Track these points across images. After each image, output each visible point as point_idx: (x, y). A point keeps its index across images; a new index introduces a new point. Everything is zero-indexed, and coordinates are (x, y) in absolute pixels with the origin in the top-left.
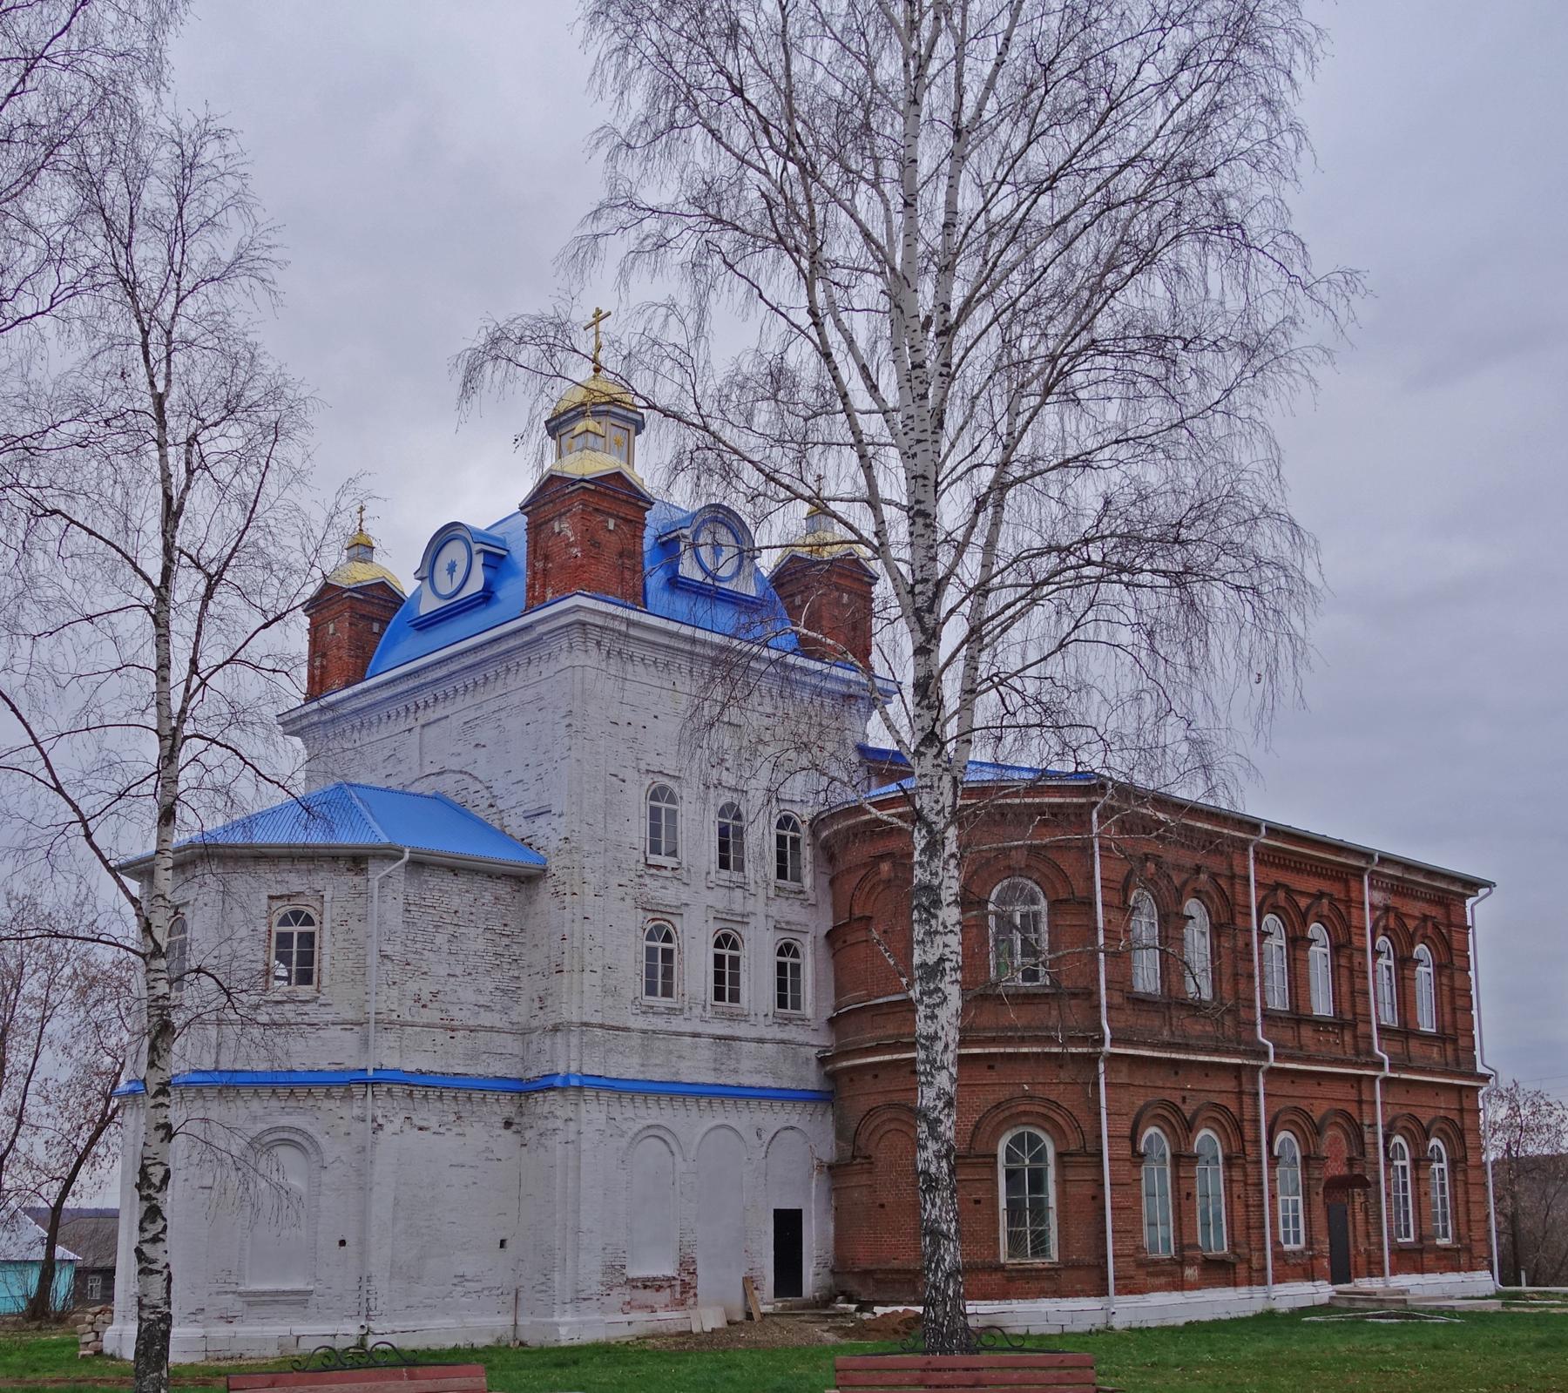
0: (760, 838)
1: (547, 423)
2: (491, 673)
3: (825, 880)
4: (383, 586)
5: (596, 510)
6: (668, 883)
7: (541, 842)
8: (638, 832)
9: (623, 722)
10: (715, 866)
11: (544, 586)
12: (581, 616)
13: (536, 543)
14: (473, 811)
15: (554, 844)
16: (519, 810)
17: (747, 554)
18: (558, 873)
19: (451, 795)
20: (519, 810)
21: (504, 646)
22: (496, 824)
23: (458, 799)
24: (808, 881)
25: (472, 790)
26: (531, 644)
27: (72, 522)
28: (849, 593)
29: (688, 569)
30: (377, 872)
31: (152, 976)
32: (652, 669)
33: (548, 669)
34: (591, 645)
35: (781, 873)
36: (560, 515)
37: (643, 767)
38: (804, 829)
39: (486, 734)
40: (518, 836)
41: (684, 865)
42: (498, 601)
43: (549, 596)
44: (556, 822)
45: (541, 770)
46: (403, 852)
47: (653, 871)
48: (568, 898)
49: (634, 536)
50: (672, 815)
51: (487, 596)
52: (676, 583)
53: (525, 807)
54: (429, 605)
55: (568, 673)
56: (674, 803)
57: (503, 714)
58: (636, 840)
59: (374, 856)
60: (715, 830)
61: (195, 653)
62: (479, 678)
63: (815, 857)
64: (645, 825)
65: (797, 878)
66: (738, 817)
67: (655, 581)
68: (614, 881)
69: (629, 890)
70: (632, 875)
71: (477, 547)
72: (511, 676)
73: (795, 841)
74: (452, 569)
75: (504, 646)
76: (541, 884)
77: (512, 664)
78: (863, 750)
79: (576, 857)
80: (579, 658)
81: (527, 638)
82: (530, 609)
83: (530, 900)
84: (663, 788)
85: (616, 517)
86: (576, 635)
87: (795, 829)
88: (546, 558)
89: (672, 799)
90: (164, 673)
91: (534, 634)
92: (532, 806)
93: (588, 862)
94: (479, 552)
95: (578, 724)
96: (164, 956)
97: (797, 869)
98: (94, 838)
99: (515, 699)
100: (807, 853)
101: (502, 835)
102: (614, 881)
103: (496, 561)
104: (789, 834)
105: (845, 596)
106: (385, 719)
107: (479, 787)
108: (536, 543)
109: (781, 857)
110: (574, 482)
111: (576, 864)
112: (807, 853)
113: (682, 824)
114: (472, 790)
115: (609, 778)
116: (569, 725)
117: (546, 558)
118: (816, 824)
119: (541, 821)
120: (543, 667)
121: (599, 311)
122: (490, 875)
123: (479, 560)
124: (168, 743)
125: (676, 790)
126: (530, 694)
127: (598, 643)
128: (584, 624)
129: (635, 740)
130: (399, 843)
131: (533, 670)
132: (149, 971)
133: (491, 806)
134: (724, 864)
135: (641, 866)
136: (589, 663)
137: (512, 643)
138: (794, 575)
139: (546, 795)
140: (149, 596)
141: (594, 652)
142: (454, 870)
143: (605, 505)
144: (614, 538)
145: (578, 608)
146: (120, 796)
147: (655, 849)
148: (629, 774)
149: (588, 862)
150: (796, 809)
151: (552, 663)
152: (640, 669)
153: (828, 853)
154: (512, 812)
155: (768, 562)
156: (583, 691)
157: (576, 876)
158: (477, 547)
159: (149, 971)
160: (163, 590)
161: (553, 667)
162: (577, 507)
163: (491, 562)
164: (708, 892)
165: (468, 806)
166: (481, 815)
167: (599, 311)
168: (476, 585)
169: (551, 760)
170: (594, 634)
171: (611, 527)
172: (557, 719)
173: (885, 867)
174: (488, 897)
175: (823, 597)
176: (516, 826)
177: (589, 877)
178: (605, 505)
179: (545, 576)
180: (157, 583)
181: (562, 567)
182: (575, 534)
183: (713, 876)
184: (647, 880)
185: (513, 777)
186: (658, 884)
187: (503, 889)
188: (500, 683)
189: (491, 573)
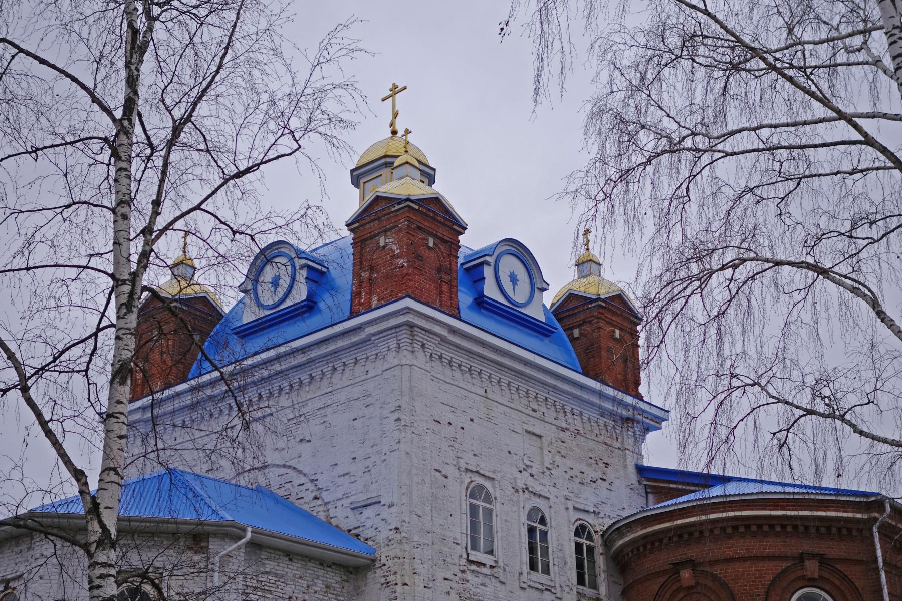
0: (561, 543)
1: (352, 171)
2: (316, 373)
3: (618, 589)
4: (204, 301)
5: (419, 228)
6: (487, 581)
7: (370, 533)
8: (460, 528)
9: (444, 421)
10: (526, 568)
11: (370, 294)
12: (410, 318)
13: (362, 255)
14: (297, 503)
15: (385, 534)
16: (346, 502)
17: (538, 285)
18: (389, 563)
19: (274, 488)
20: (346, 502)
21: (332, 347)
22: (322, 516)
23: (281, 493)
24: (603, 590)
25: (296, 482)
26: (362, 345)
27: (21, 50)
28: (621, 329)
29: (490, 291)
30: (219, 549)
31: (98, 571)
32: (467, 375)
33: (375, 368)
34: (417, 346)
35: (581, 581)
36: (386, 231)
37: (463, 465)
38: (597, 538)
39: (312, 428)
40: (345, 526)
41: (501, 563)
42: (320, 311)
43: (375, 303)
44: (385, 513)
45: (368, 463)
46: (244, 530)
47: (473, 567)
48: (399, 589)
49: (450, 255)
50: (489, 513)
51: (309, 306)
52: (481, 303)
53: (352, 499)
54: (248, 317)
55: (397, 371)
56: (489, 502)
57: (329, 411)
58: (458, 536)
59: (215, 535)
60: (524, 531)
61: (159, 194)
62: (305, 377)
63: (607, 565)
64: (466, 520)
65: (594, 586)
66: (543, 521)
67: (465, 299)
68: (440, 575)
69: (454, 585)
70: (456, 570)
71: (299, 263)
72: (337, 375)
73: (590, 550)
74: (275, 283)
75: (332, 347)
76: (370, 575)
77: (338, 364)
78: (642, 470)
79: (407, 547)
80: (406, 357)
81: (355, 339)
82: (353, 314)
83: (358, 591)
84: (481, 487)
85: (435, 236)
86: (404, 335)
87: (590, 538)
88: (372, 269)
89: (488, 499)
90: (124, 210)
91: (362, 335)
92: (361, 498)
93: (417, 552)
94: (302, 268)
95: (406, 418)
96: (113, 545)
97: (594, 576)
98: (32, 392)
99: (342, 397)
100: (600, 561)
101: (328, 526)
102: (440, 575)
103: (318, 276)
104: (585, 542)
105: (617, 332)
106: (207, 417)
107: (303, 480)
108: (362, 255)
109: (580, 565)
110: (399, 201)
111: (407, 555)
112: (600, 561)
113: (497, 524)
114: (296, 482)
115: (434, 473)
116: (398, 420)
117: (372, 269)
118: (608, 537)
119: (369, 512)
120: (369, 366)
121: (395, 86)
122: (322, 563)
123: (302, 275)
124: (127, 288)
125: (491, 490)
126: (357, 391)
127: (423, 346)
128: (411, 326)
129: (455, 439)
130: (241, 521)
131: (359, 369)
132: (93, 565)
133: (316, 498)
134: (533, 567)
135: (463, 562)
136: (415, 362)
137: (340, 343)
138: (572, 307)
139: (374, 486)
140: (107, 128)
141: (420, 354)
142: (289, 555)
143: (426, 224)
144: (432, 255)
145: (408, 310)
146: (43, 368)
147: (475, 547)
148: (451, 471)
149: (417, 552)
150: (591, 519)
151: (379, 362)
152: (457, 374)
153: (621, 563)
154: (339, 504)
155: (549, 299)
156: (411, 389)
157: (407, 567)
158: (299, 263)
159: (93, 565)
160: (126, 123)
161: (380, 366)
162: (403, 224)
163: (315, 276)
164: (521, 593)
165: (292, 499)
166: (306, 507)
167: (395, 86)
168: (301, 293)
169: (379, 452)
170: (420, 336)
171: (431, 245)
172: (386, 413)
173: (686, 574)
174: (320, 585)
175: (599, 335)
176: (343, 518)
177: (419, 568)
178: (426, 224)
179: (371, 284)
180: (118, 114)
181: (387, 277)
182: (401, 248)
183: (525, 578)
184: (469, 576)
185: (340, 470)
186: (480, 580)
187: (333, 578)
188: (325, 381)
189: (314, 286)
